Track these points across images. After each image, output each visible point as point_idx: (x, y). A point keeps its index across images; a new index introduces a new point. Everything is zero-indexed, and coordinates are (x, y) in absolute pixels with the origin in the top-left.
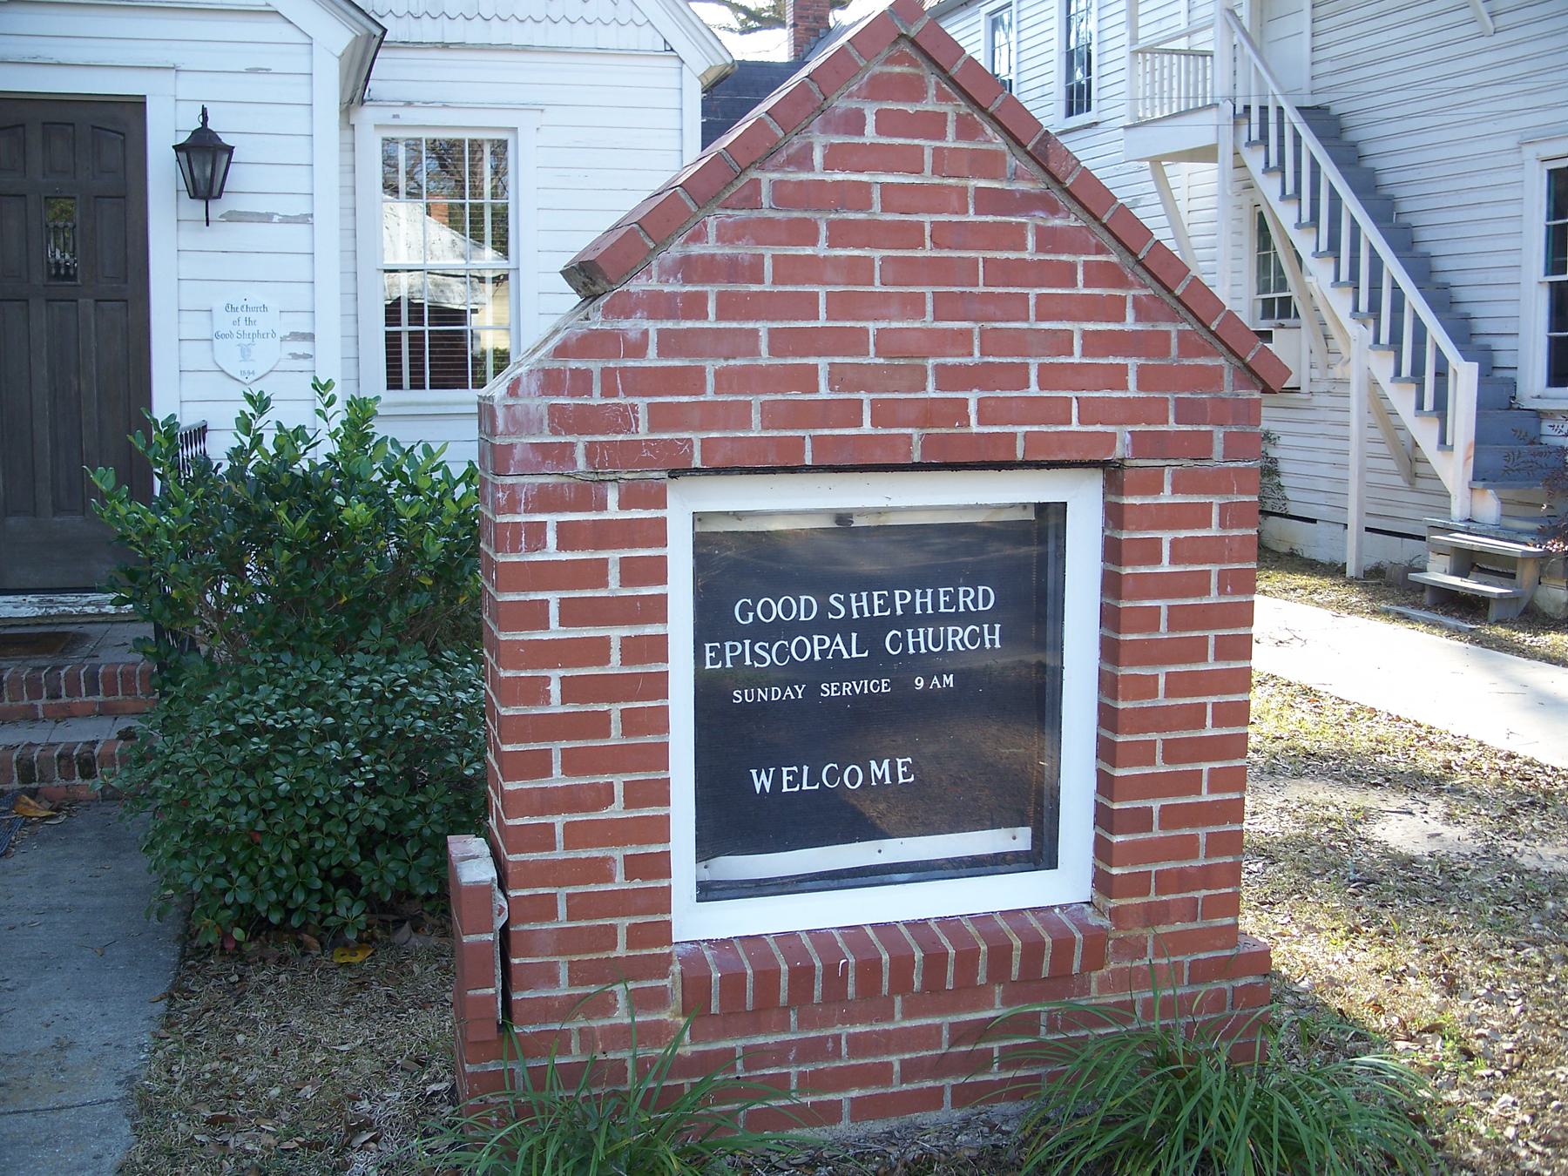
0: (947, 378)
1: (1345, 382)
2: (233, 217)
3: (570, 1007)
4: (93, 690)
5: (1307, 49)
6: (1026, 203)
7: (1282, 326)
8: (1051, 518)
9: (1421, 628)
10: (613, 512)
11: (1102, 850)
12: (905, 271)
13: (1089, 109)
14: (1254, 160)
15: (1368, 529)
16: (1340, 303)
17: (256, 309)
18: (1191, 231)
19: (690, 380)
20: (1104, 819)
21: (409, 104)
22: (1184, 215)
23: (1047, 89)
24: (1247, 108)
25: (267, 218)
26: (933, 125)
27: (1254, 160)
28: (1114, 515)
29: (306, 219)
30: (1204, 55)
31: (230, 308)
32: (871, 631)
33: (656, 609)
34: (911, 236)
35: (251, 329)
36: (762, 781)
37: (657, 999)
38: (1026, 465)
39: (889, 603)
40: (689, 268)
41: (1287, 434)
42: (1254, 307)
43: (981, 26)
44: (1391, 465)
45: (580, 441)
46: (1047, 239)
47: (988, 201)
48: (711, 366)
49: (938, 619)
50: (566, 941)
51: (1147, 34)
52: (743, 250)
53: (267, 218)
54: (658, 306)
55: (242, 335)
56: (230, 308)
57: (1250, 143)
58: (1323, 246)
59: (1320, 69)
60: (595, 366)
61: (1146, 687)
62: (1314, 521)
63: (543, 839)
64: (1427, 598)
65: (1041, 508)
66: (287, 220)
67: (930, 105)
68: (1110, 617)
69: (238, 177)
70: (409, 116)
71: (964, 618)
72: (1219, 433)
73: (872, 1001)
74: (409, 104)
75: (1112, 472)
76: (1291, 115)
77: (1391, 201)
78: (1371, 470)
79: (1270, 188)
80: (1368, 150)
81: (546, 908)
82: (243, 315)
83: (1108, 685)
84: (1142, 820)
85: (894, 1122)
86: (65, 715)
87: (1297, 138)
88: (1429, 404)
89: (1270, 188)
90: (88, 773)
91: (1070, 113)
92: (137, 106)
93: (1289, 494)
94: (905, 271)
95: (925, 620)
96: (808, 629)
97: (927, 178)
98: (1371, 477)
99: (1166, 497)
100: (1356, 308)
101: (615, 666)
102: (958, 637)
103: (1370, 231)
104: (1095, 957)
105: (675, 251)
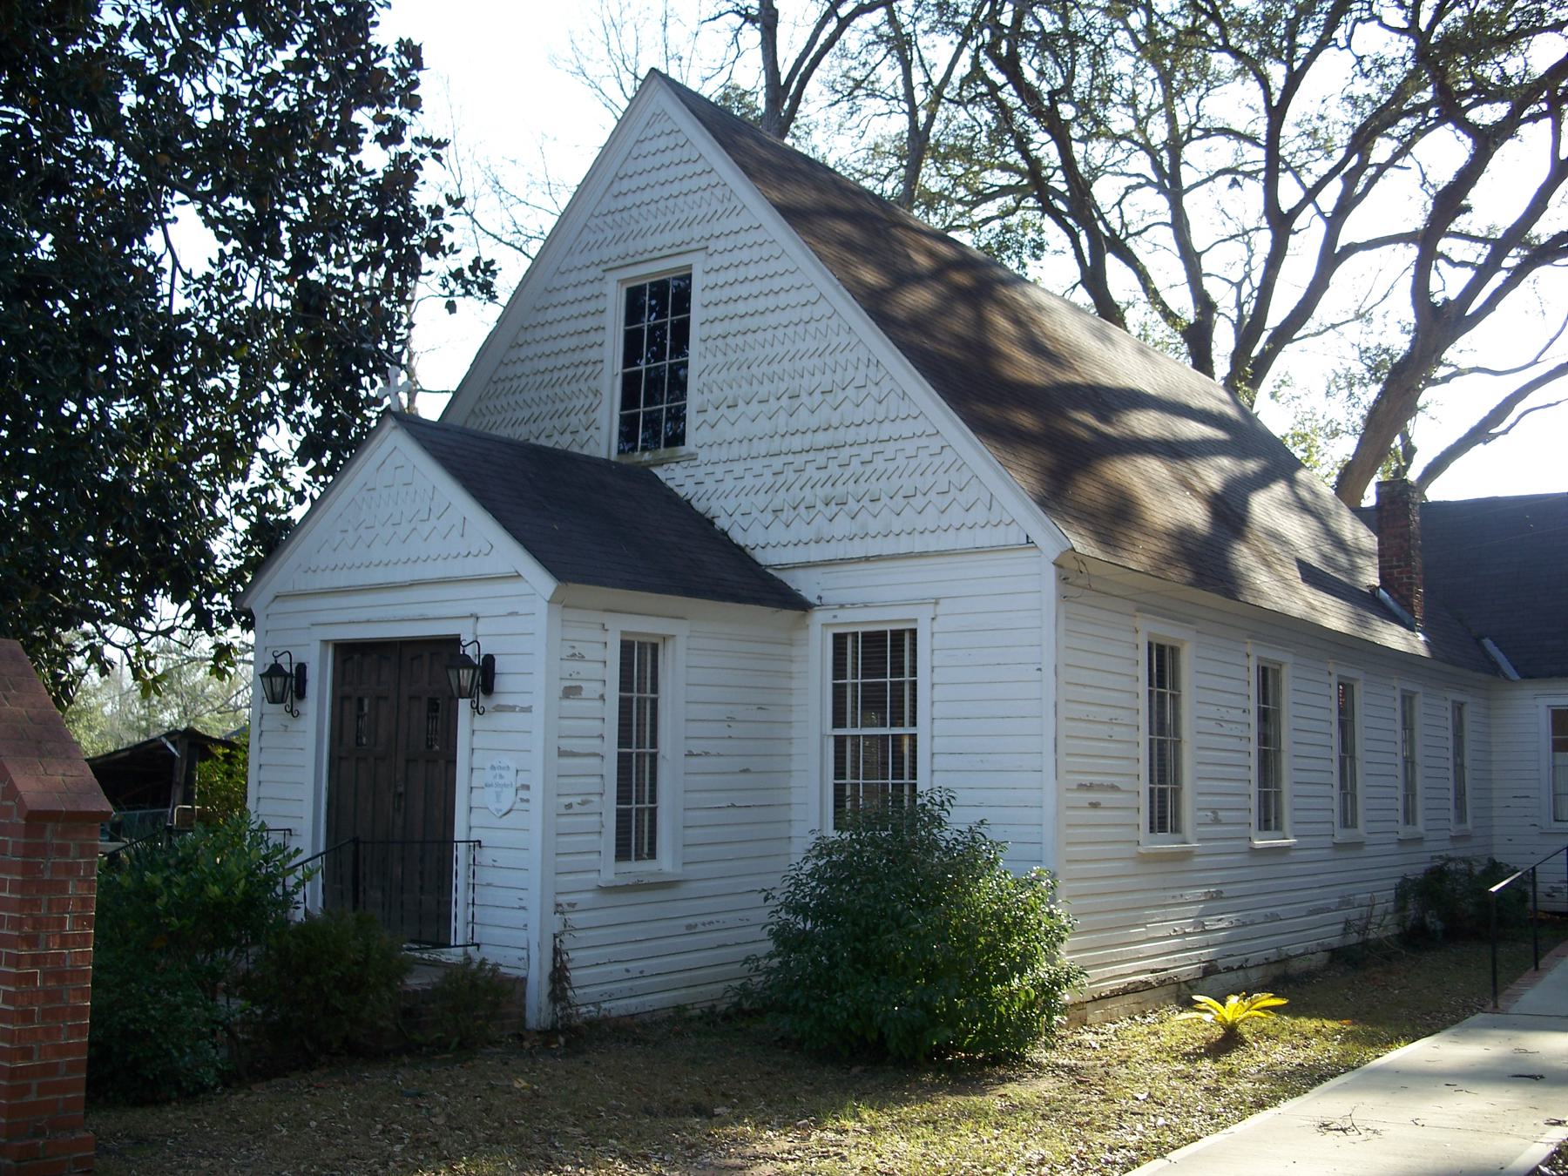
2: (501, 709)
9: (928, 1078)
17: (503, 769)
21: (842, 606)
25: (512, 709)
35: (501, 782)
53: (512, 709)
55: (498, 785)
56: (493, 768)
69: (501, 683)
70: (845, 616)
74: (842, 606)
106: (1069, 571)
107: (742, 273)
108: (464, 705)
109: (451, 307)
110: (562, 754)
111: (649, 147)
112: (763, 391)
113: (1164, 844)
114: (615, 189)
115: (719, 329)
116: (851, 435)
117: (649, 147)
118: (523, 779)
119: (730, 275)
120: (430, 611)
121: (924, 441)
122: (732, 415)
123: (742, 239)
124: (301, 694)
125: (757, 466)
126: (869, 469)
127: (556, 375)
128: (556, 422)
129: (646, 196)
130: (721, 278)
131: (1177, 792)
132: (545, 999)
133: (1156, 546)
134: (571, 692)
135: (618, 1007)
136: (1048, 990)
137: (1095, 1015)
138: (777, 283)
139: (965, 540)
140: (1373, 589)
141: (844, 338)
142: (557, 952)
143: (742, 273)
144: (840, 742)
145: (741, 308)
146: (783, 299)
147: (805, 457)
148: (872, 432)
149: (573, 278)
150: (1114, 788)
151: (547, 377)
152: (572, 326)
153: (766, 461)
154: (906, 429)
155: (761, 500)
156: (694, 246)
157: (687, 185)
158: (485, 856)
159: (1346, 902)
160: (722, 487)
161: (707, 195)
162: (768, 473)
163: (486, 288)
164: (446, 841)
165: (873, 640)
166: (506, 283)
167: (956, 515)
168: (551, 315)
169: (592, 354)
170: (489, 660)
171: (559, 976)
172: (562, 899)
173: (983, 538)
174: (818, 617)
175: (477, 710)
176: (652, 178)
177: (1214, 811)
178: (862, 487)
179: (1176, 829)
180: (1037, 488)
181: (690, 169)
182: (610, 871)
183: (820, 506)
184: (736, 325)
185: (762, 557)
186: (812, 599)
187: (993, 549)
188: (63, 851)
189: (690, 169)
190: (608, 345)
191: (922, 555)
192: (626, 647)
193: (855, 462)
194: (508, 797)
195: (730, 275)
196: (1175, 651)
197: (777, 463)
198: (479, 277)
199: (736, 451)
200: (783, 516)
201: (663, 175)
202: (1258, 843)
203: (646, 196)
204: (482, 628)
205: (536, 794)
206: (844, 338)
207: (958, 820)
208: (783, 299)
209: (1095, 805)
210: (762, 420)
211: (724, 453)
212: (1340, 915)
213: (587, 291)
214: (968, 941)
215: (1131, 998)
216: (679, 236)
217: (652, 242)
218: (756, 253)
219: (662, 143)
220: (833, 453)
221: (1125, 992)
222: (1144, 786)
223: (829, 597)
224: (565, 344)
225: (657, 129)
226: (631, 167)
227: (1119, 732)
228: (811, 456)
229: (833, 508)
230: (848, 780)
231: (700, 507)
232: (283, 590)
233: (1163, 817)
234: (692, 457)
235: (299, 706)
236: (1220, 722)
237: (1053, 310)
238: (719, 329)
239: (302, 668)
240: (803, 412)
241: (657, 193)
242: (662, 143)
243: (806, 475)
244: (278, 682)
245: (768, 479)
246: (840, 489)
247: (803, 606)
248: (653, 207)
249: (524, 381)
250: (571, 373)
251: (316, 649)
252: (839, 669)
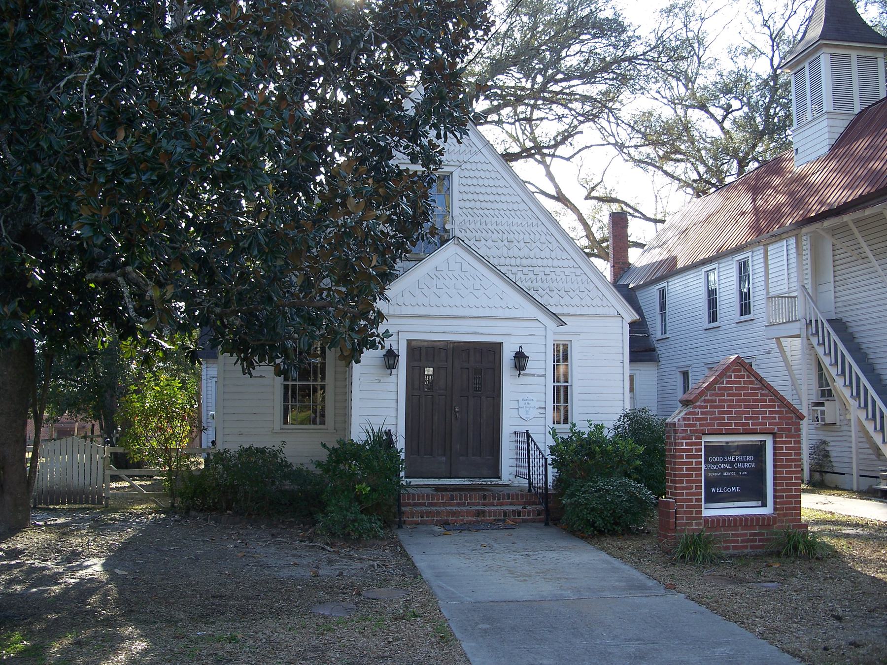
0: (746, 418)
1: (850, 420)
2: (525, 375)
3: (686, 524)
4: (508, 498)
5: (833, 298)
6: (758, 389)
7: (828, 400)
8: (762, 446)
10: (694, 440)
11: (775, 503)
12: (738, 401)
13: (750, 314)
14: (814, 341)
15: (861, 476)
16: (847, 393)
18: (791, 363)
19: (706, 419)
20: (775, 497)
22: (789, 357)
23: (732, 304)
24: (811, 321)
25: (533, 375)
26: (743, 377)
27: (814, 341)
28: (775, 442)
29: (544, 376)
30: (795, 297)
31: (524, 400)
32: (732, 463)
33: (700, 456)
34: (740, 395)
36: (713, 490)
37: (699, 524)
38: (759, 433)
39: (735, 459)
40: (705, 401)
41: (832, 441)
42: (818, 393)
43: (703, 276)
44: (870, 451)
45: (689, 429)
46: (762, 395)
47: (752, 389)
48: (709, 417)
49: (743, 462)
50: (685, 513)
51: (773, 291)
52: (713, 398)
53: (533, 375)
54: (700, 407)
55: (527, 407)
56: (524, 400)
57: (812, 334)
58: (840, 372)
59: (839, 304)
60: (691, 417)
61: (782, 472)
62: (844, 474)
63: (682, 494)
64: (879, 495)
65: (761, 441)
66: (539, 376)
67: (742, 373)
68: (775, 460)
69: (530, 364)
71: (748, 462)
72: (793, 428)
73: (735, 527)
75: (774, 435)
76: (826, 324)
77: (866, 354)
78: (860, 453)
79: (820, 351)
80: (857, 335)
81: (682, 506)
82: (527, 402)
83: (775, 472)
84: (782, 497)
85: (740, 551)
86: (502, 504)
87: (829, 334)
88: (878, 428)
89: (820, 351)
90: (519, 516)
91: (742, 315)
92: (500, 344)
93: (834, 464)
94: (738, 401)
95: (741, 462)
96: (722, 463)
97: (742, 385)
98: (861, 456)
99: (784, 439)
100: (852, 394)
101: (694, 466)
102: (747, 465)
103: (855, 368)
104: (775, 523)
105: (703, 398)
120: (481, 330)
173: (599, 311)
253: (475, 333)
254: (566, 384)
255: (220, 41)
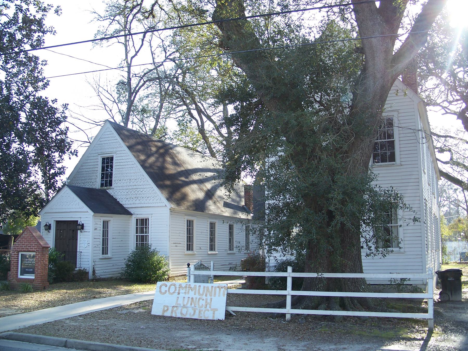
2: (84, 232)
25: (87, 232)
26: (28, 233)
34: (27, 239)
53: (87, 232)
54: (18, 243)
69: (84, 228)
70: (138, 216)
106: (172, 210)
107: (122, 158)
108: (79, 231)
109: (70, 158)
110: (95, 238)
111: (106, 133)
112: (125, 178)
113: (190, 252)
114: (100, 140)
115: (118, 167)
116: (139, 187)
117: (106, 133)
118: (88, 242)
119: (120, 158)
120: (73, 216)
121: (150, 189)
122: (120, 182)
123: (122, 152)
124: (50, 229)
125: (124, 191)
126: (142, 193)
127: (89, 172)
128: (89, 180)
129: (106, 142)
130: (118, 158)
131: (193, 244)
132: (92, 275)
133: (189, 204)
134: (96, 229)
135: (103, 277)
136: (164, 273)
137: (176, 278)
138: (128, 160)
139: (156, 205)
140: (243, 206)
141: (138, 171)
142: (93, 268)
143: (122, 158)
144: (137, 236)
145: (122, 164)
146: (129, 163)
147: (132, 190)
148: (142, 187)
149: (93, 155)
150: (180, 243)
151: (88, 172)
152: (92, 164)
153: (126, 190)
154: (148, 186)
155: (125, 197)
156: (114, 152)
157: (113, 141)
158: (82, 254)
159: (230, 264)
160: (118, 194)
161: (116, 143)
162: (126, 192)
163: (76, 155)
164: (76, 252)
165: (142, 220)
166: (80, 155)
167: (155, 201)
168: (88, 161)
169: (96, 169)
170: (83, 224)
171: (94, 271)
172: (94, 260)
173: (159, 205)
174: (133, 216)
175: (81, 232)
176: (107, 139)
177: (200, 247)
178: (141, 196)
179: (192, 250)
180: (168, 196)
181: (113, 138)
182: (101, 256)
183: (134, 198)
184: (121, 167)
185: (125, 206)
186: (133, 213)
187: (160, 207)
188: (45, 251)
189: (113, 138)
190: (99, 168)
191: (150, 207)
192: (104, 222)
193: (140, 191)
194: (86, 245)
195: (120, 158)
196: (193, 221)
197: (127, 191)
198: (75, 153)
199: (121, 188)
200: (128, 199)
201: (109, 139)
202: (209, 253)
203: (106, 142)
204: (82, 219)
205: (91, 245)
206: (138, 171)
207: (153, 248)
208: (129, 163)
209: (176, 246)
210: (125, 183)
211: (118, 188)
212: (230, 266)
213: (95, 158)
214: (152, 264)
215: (183, 277)
216: (111, 150)
217: (107, 150)
218: (124, 155)
219: (109, 133)
220: (136, 190)
221: (182, 276)
222: (186, 243)
223: (135, 213)
224: (91, 167)
225: (108, 130)
226: (103, 137)
227: (181, 235)
228: (133, 190)
229: (136, 199)
230: (138, 242)
231: (114, 197)
232: (47, 212)
233: (190, 247)
234: (113, 188)
235: (50, 231)
236: (202, 233)
237: (182, 152)
238: (118, 167)
239: (50, 224)
240: (132, 183)
241: (107, 142)
242: (109, 133)
243: (132, 193)
244: (47, 227)
245: (126, 193)
246: (137, 195)
247: (131, 214)
248: (107, 144)
249: (83, 173)
250: (92, 172)
251: (53, 221)
252: (137, 225)
253: (72, 217)
254: (137, 234)
255: (20, 125)
